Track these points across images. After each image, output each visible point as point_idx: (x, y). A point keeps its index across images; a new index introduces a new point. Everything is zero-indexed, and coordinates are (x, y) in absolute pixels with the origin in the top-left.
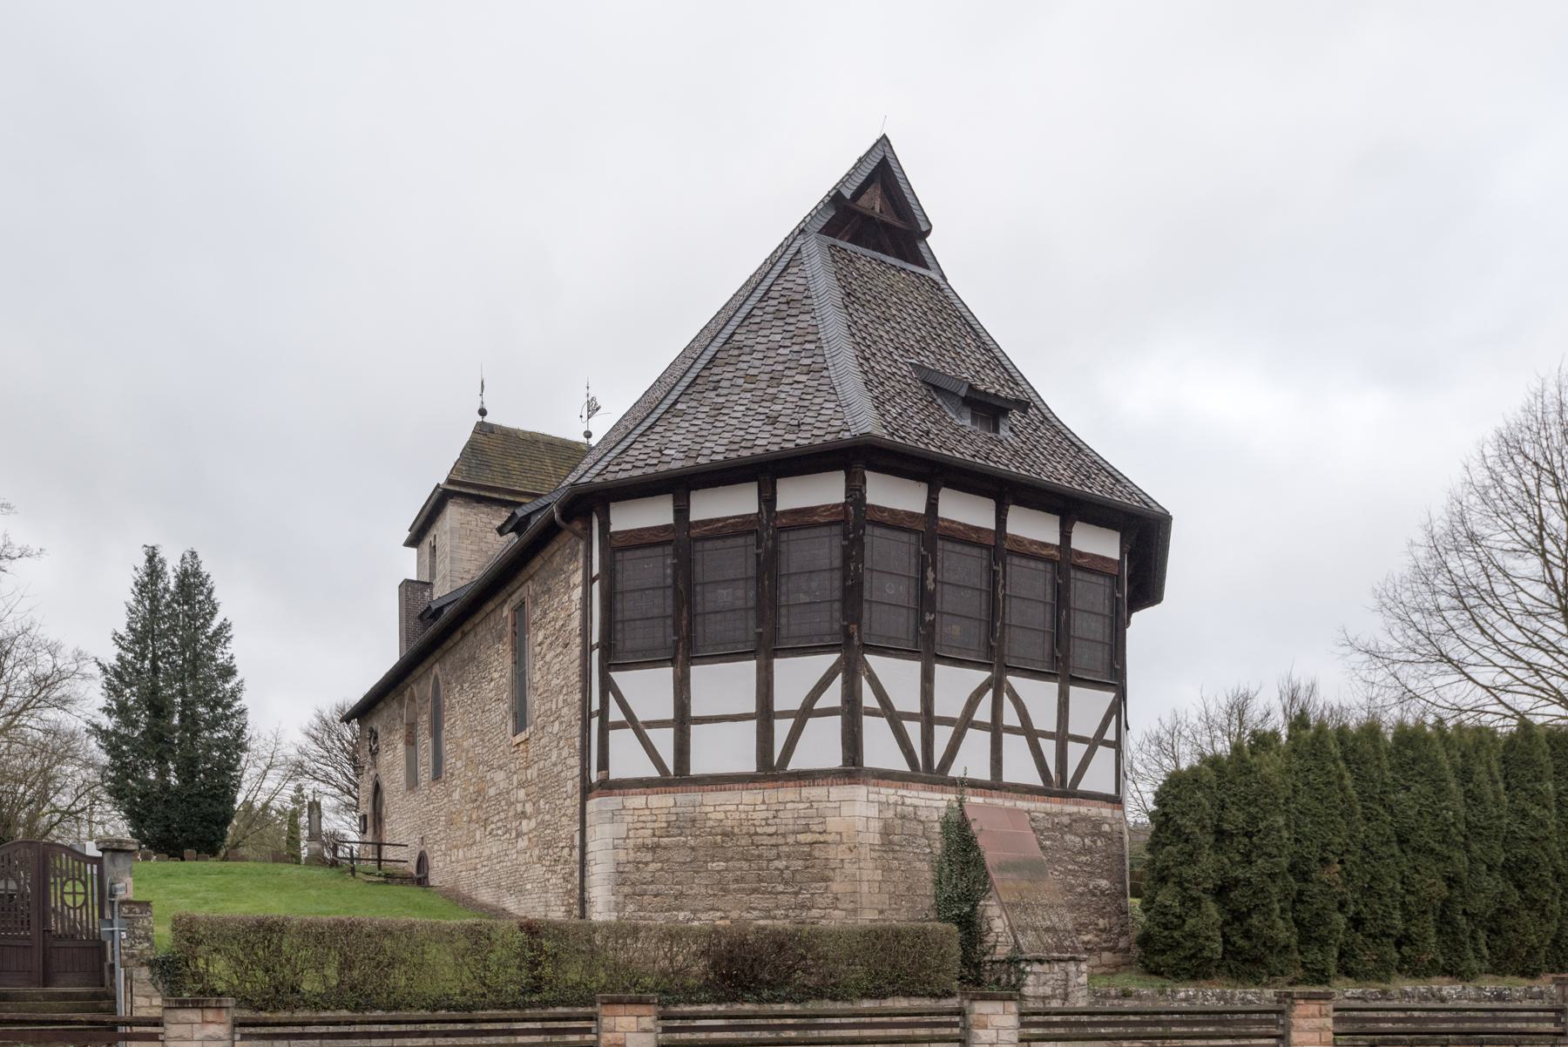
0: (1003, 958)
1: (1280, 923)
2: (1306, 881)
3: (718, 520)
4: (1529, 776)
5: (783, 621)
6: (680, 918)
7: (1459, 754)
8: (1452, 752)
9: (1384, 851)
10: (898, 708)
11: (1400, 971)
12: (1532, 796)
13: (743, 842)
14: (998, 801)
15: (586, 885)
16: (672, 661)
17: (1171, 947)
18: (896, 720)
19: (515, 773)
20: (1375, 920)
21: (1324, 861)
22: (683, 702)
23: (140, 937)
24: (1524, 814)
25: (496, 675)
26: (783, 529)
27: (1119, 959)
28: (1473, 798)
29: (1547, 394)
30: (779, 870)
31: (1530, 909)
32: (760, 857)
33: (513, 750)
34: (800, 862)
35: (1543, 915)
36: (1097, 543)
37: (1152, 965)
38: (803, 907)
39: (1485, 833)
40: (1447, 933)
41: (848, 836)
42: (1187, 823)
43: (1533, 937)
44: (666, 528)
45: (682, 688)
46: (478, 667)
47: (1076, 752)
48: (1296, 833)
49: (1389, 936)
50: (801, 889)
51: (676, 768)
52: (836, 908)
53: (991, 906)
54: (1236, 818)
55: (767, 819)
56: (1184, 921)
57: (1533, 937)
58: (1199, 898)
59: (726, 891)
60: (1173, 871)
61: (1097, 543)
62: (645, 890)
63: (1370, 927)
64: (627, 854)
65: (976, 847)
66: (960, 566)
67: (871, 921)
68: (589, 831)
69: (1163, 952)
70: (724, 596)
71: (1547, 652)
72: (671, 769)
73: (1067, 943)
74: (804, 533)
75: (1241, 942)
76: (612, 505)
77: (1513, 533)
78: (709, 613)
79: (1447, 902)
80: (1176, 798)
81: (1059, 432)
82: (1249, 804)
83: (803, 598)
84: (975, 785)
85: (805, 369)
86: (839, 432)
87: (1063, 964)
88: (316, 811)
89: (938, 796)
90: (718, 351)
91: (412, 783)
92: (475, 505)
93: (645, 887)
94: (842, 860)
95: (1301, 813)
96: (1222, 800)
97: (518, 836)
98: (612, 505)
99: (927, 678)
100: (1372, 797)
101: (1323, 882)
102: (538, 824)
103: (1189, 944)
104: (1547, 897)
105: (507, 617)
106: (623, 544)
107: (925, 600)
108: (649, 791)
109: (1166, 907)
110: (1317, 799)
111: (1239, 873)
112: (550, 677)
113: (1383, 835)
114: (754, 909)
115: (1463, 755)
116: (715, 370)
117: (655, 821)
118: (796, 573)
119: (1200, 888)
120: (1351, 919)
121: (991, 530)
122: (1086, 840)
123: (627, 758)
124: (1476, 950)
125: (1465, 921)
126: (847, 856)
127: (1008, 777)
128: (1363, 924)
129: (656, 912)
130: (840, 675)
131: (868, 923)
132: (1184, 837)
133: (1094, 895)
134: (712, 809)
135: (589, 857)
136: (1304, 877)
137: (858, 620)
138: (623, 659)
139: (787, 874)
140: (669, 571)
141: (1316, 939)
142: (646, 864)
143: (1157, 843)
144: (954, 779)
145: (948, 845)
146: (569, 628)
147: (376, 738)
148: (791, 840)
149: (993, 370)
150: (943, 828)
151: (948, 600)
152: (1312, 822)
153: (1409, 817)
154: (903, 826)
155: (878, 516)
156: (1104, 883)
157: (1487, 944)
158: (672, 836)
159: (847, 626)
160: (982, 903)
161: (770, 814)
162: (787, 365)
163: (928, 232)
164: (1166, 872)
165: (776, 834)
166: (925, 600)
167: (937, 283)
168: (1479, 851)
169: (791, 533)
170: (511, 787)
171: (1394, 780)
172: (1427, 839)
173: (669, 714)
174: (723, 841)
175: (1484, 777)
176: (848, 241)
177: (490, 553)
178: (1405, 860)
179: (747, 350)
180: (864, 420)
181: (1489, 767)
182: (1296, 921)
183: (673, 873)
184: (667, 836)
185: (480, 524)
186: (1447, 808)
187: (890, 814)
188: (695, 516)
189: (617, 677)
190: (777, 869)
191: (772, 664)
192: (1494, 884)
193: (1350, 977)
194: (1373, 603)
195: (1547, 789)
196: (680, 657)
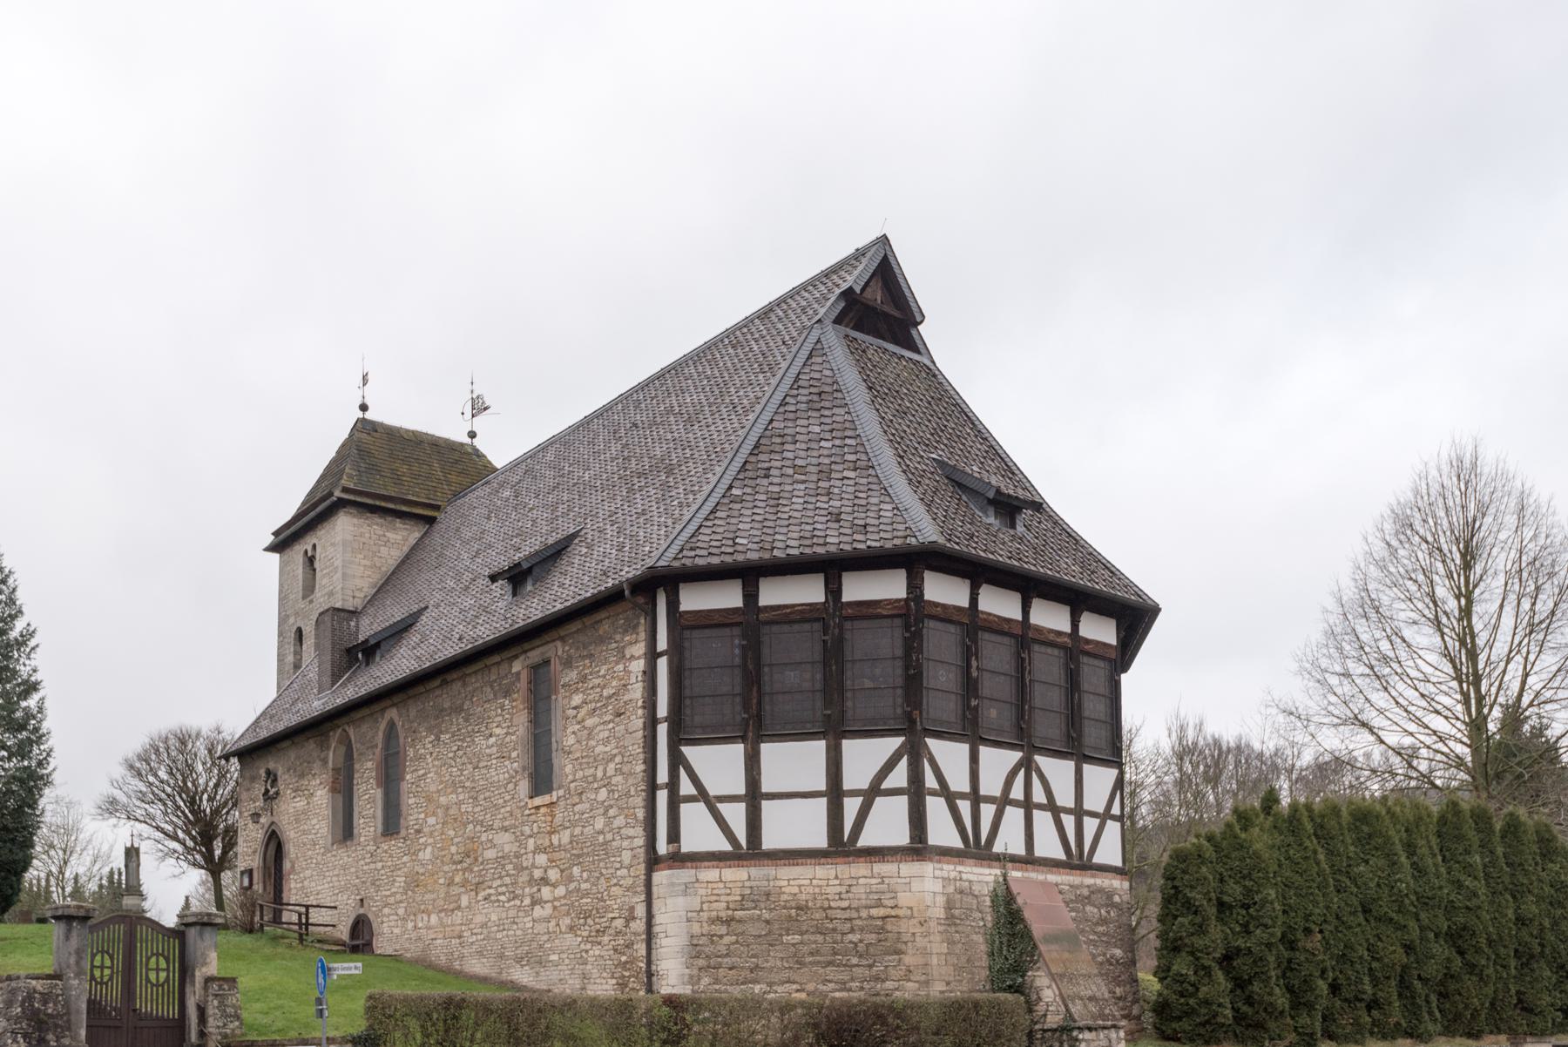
0: (1055, 1026)
1: (1277, 991)
2: (1293, 949)
3: (786, 606)
4: (1461, 850)
5: (849, 704)
6: (756, 991)
7: (1403, 829)
8: (1398, 827)
9: (1350, 920)
10: (1049, 814)
11: (1372, 1033)
12: (1465, 868)
13: (817, 916)
14: (1033, 875)
15: (654, 957)
16: (743, 739)
17: (1187, 1014)
18: (951, 798)
19: (531, 836)
20: (1349, 985)
21: (1307, 931)
22: (754, 778)
23: (231, 1016)
24: (1459, 885)
25: (497, 731)
26: (848, 618)
27: (1133, 1027)
28: (1419, 870)
29: (1430, 477)
30: (853, 943)
31: (1471, 974)
32: (834, 930)
33: (527, 812)
34: (873, 936)
35: (1481, 979)
36: (1097, 630)
37: (1170, 1031)
38: (878, 979)
39: (1431, 903)
40: (1407, 997)
41: (919, 910)
42: (1196, 896)
43: (1475, 1000)
44: (735, 610)
45: (752, 764)
46: (466, 720)
47: (1090, 825)
48: (1284, 905)
49: (1361, 1000)
50: (875, 961)
51: (748, 842)
52: (909, 980)
53: (1040, 976)
54: (1234, 891)
55: (840, 894)
56: (1197, 989)
57: (1475, 1000)
58: (1210, 967)
59: (801, 964)
60: (1187, 941)
61: (1097, 630)
62: (720, 963)
63: (1346, 993)
64: (701, 927)
65: (1023, 920)
66: (996, 655)
67: (942, 992)
68: (657, 905)
69: (1179, 1019)
70: (791, 677)
71: (1446, 718)
72: (743, 842)
73: (1107, 1011)
74: (864, 624)
75: (1245, 1008)
76: (681, 585)
77: (1409, 603)
78: (777, 693)
79: (1405, 968)
80: (1184, 872)
81: (1056, 523)
82: (1244, 878)
83: (868, 684)
84: (1014, 859)
85: (851, 465)
86: (906, 537)
87: (1106, 1032)
88: (134, 859)
89: (987, 871)
90: (760, 437)
91: (345, 831)
92: (369, 515)
93: (720, 959)
94: (914, 934)
95: (1286, 886)
96: (1221, 874)
97: (534, 903)
98: (681, 585)
99: (974, 759)
100: (1339, 870)
101: (1308, 951)
102: (569, 893)
103: (1204, 1011)
104: (1483, 962)
105: (518, 674)
106: (693, 623)
107: (970, 687)
108: (722, 864)
109: (1182, 975)
110: (1297, 872)
111: (1240, 943)
112: (593, 743)
113: (1351, 906)
114: (830, 981)
115: (1407, 831)
116: (762, 457)
117: (729, 895)
118: (860, 660)
119: (1211, 957)
120: (1330, 985)
121: (1018, 621)
122: (1102, 911)
123: (699, 831)
124: (1430, 1013)
125: (1420, 986)
126: (918, 930)
127: (1039, 852)
128: (1340, 989)
129: (732, 984)
130: (905, 757)
131: (938, 994)
132: (1194, 909)
133: (1111, 964)
134: (786, 883)
135: (656, 929)
136: (1292, 946)
137: (918, 705)
138: (692, 734)
139: (861, 947)
140: (737, 651)
141: (1305, 1004)
142: (721, 937)
143: (1167, 915)
144: (998, 855)
145: (998, 917)
146: (626, 698)
147: (275, 781)
148: (864, 914)
149: (993, 460)
150: (992, 901)
151: (988, 686)
152: (1295, 894)
153: (1369, 888)
154: (961, 900)
155: (933, 611)
156: (1118, 952)
157: (1438, 1007)
158: (747, 909)
159: (911, 712)
160: (1030, 973)
161: (843, 889)
162: (832, 459)
163: (922, 322)
164: (1179, 942)
165: (849, 908)
166: (970, 687)
167: (930, 369)
168: (1427, 920)
169: (855, 623)
170: (523, 851)
171: (1356, 853)
172: (1386, 909)
173: (741, 790)
174: (798, 915)
175: (1425, 850)
176: (852, 329)
177: (384, 569)
178: (1369, 928)
179: (789, 439)
180: (928, 531)
181: (1429, 842)
182: (1287, 988)
183: (748, 946)
184: (742, 910)
185: (374, 537)
186: (1400, 880)
187: (951, 889)
188: (764, 601)
189: (688, 751)
190: (851, 942)
191: (840, 744)
192: (1441, 950)
193: (1332, 1040)
194: (1295, 666)
195: (1475, 862)
196: (751, 734)
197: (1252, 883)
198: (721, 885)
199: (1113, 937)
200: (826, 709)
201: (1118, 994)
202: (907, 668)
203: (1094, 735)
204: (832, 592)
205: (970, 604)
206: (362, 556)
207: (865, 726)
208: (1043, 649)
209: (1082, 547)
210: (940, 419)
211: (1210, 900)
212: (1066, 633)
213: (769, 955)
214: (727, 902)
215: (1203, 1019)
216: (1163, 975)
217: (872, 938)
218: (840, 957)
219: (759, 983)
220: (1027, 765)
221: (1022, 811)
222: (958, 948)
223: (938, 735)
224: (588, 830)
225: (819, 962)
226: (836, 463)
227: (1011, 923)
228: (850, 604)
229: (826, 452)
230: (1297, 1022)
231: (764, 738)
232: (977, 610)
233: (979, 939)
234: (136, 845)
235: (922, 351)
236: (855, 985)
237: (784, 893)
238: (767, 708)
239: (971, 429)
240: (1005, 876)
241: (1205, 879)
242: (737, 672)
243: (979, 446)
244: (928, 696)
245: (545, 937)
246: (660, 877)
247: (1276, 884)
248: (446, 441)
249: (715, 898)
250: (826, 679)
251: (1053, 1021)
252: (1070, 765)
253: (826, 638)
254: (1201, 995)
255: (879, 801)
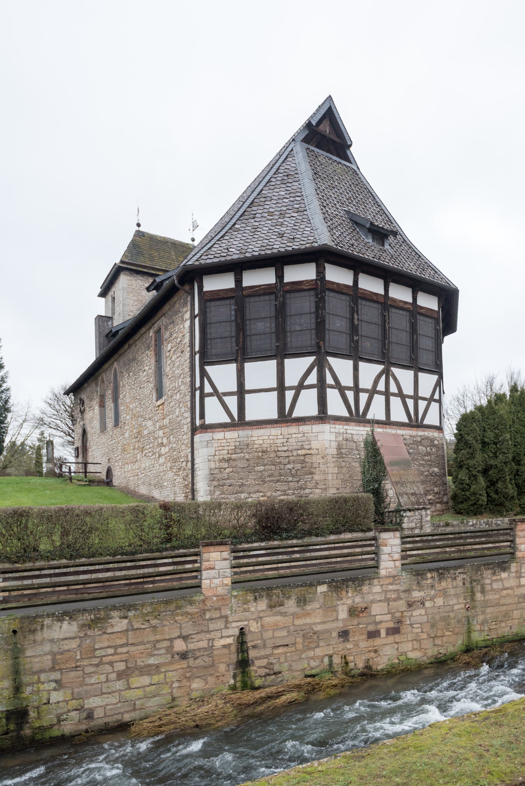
1: (510, 486)
2: (519, 465)
5: (289, 339)
6: (242, 497)
13: (272, 455)
15: (195, 482)
16: (235, 360)
18: (342, 390)
27: (444, 507)
32: (280, 463)
34: (300, 465)
37: (458, 509)
38: (301, 488)
44: (231, 290)
47: (422, 405)
48: (515, 442)
50: (300, 479)
51: (239, 417)
52: (317, 488)
54: (490, 435)
55: (283, 443)
56: (470, 487)
58: (476, 475)
59: (264, 482)
60: (465, 462)
62: (225, 483)
64: (215, 464)
65: (380, 454)
68: (196, 452)
69: (462, 502)
74: (297, 294)
76: (204, 277)
80: (465, 427)
81: (410, 247)
82: (495, 429)
83: (298, 328)
84: (378, 422)
85: (296, 210)
87: (419, 511)
88: (50, 446)
89: (362, 428)
91: (103, 428)
92: (135, 275)
93: (224, 481)
94: (319, 463)
95: (516, 432)
96: (484, 427)
98: (204, 277)
99: (356, 369)
105: (152, 336)
107: (354, 329)
108: (225, 430)
109: (462, 480)
111: (492, 462)
114: (278, 490)
116: (254, 208)
117: (229, 446)
119: (476, 470)
121: (382, 295)
122: (428, 449)
126: (321, 461)
127: (393, 419)
130: (316, 367)
132: (469, 446)
133: (432, 476)
137: (323, 339)
138: (211, 359)
140: (233, 313)
142: (225, 469)
144: (369, 420)
147: (83, 403)
148: (295, 453)
149: (381, 216)
150: (365, 445)
151: (364, 329)
152: (520, 437)
155: (331, 286)
156: (436, 470)
160: (383, 482)
161: (285, 440)
162: (287, 208)
164: (462, 463)
166: (354, 329)
167: (355, 171)
173: (235, 389)
174: (262, 455)
177: (143, 302)
179: (269, 199)
183: (238, 473)
184: (235, 454)
187: (340, 438)
190: (288, 469)
196: (239, 358)
197: (498, 431)
198: (225, 441)
199: (434, 462)
200: (276, 343)
201: (436, 491)
202: (317, 318)
203: (425, 358)
204: (279, 277)
205: (353, 284)
206: (132, 295)
207: (296, 351)
208: (397, 311)
209: (422, 259)
210: (355, 193)
211: (477, 440)
212: (410, 303)
213: (248, 478)
214: (228, 450)
215: (473, 502)
216: (455, 480)
217: (299, 466)
218: (283, 477)
219: (243, 493)
220: (387, 372)
221: (384, 397)
222: (344, 470)
223: (335, 355)
224: (174, 416)
225: (273, 480)
226: (289, 209)
227: (375, 456)
228: (288, 283)
229: (285, 204)
230: (521, 502)
231: (246, 360)
232: (358, 288)
233: (357, 465)
234: (51, 439)
235: (353, 162)
236: (290, 492)
237: (256, 444)
238: (249, 343)
239: (372, 200)
240: (372, 431)
241: (475, 430)
242: (233, 324)
243: (375, 208)
244: (329, 333)
245: (163, 474)
246: (197, 438)
247: (510, 431)
248: (180, 242)
249: (221, 448)
250: (277, 327)
251: (393, 506)
252: (411, 373)
253: (277, 303)
254: (471, 490)
255: (303, 392)
